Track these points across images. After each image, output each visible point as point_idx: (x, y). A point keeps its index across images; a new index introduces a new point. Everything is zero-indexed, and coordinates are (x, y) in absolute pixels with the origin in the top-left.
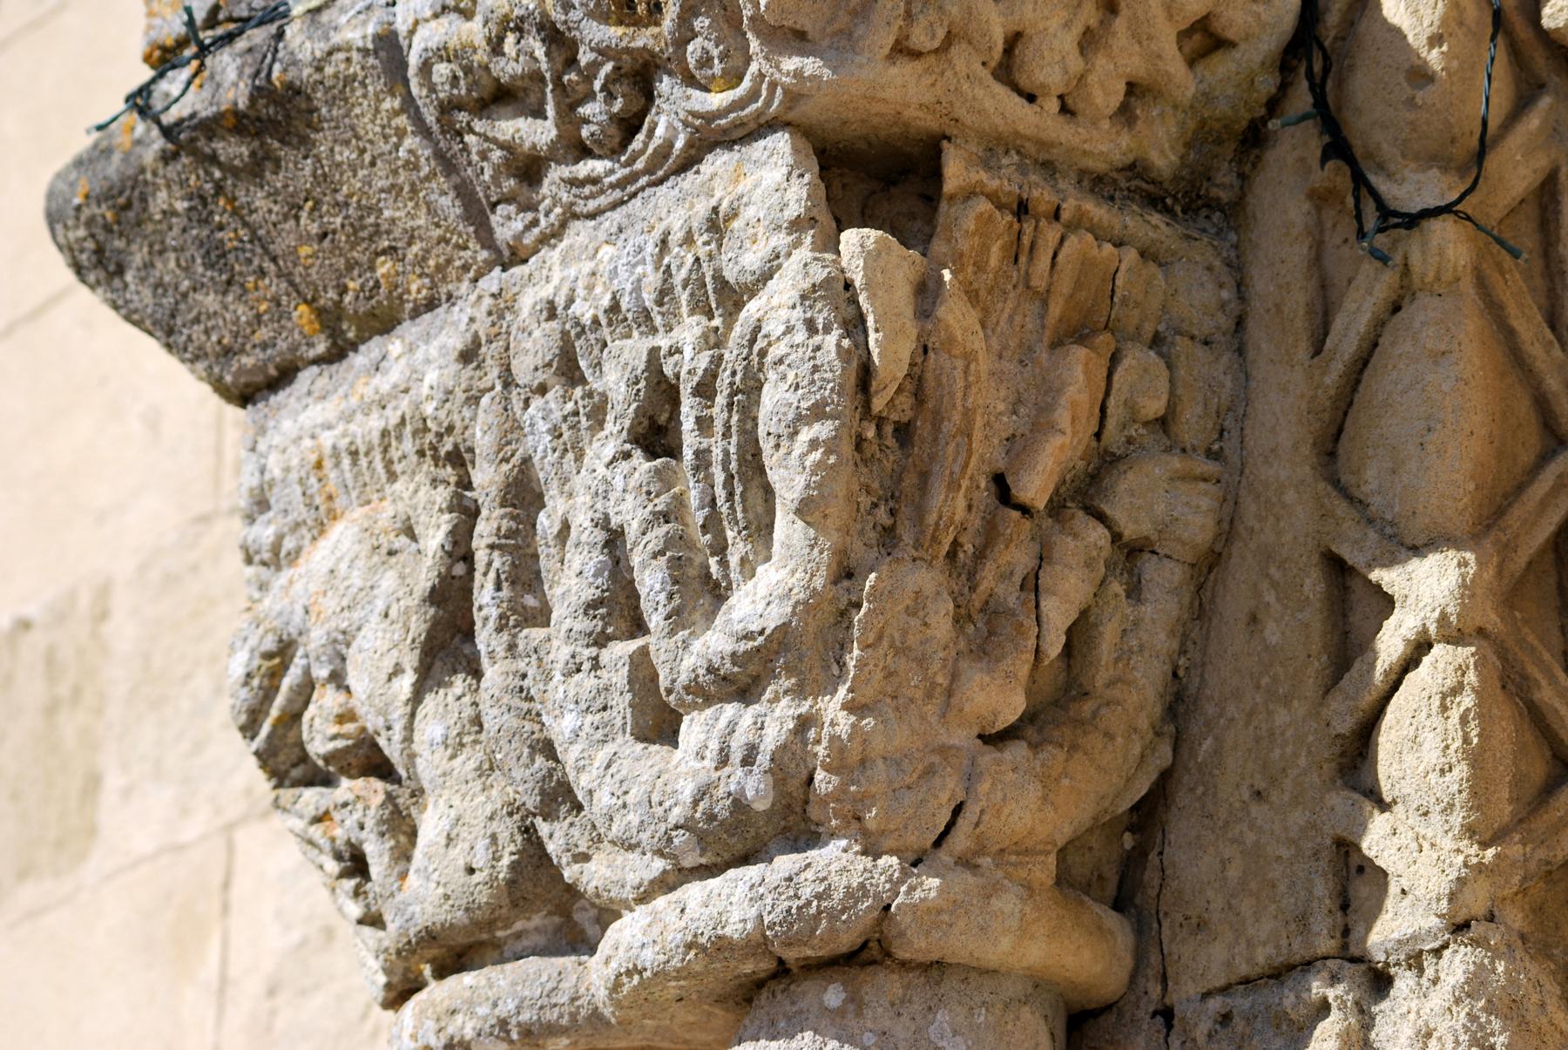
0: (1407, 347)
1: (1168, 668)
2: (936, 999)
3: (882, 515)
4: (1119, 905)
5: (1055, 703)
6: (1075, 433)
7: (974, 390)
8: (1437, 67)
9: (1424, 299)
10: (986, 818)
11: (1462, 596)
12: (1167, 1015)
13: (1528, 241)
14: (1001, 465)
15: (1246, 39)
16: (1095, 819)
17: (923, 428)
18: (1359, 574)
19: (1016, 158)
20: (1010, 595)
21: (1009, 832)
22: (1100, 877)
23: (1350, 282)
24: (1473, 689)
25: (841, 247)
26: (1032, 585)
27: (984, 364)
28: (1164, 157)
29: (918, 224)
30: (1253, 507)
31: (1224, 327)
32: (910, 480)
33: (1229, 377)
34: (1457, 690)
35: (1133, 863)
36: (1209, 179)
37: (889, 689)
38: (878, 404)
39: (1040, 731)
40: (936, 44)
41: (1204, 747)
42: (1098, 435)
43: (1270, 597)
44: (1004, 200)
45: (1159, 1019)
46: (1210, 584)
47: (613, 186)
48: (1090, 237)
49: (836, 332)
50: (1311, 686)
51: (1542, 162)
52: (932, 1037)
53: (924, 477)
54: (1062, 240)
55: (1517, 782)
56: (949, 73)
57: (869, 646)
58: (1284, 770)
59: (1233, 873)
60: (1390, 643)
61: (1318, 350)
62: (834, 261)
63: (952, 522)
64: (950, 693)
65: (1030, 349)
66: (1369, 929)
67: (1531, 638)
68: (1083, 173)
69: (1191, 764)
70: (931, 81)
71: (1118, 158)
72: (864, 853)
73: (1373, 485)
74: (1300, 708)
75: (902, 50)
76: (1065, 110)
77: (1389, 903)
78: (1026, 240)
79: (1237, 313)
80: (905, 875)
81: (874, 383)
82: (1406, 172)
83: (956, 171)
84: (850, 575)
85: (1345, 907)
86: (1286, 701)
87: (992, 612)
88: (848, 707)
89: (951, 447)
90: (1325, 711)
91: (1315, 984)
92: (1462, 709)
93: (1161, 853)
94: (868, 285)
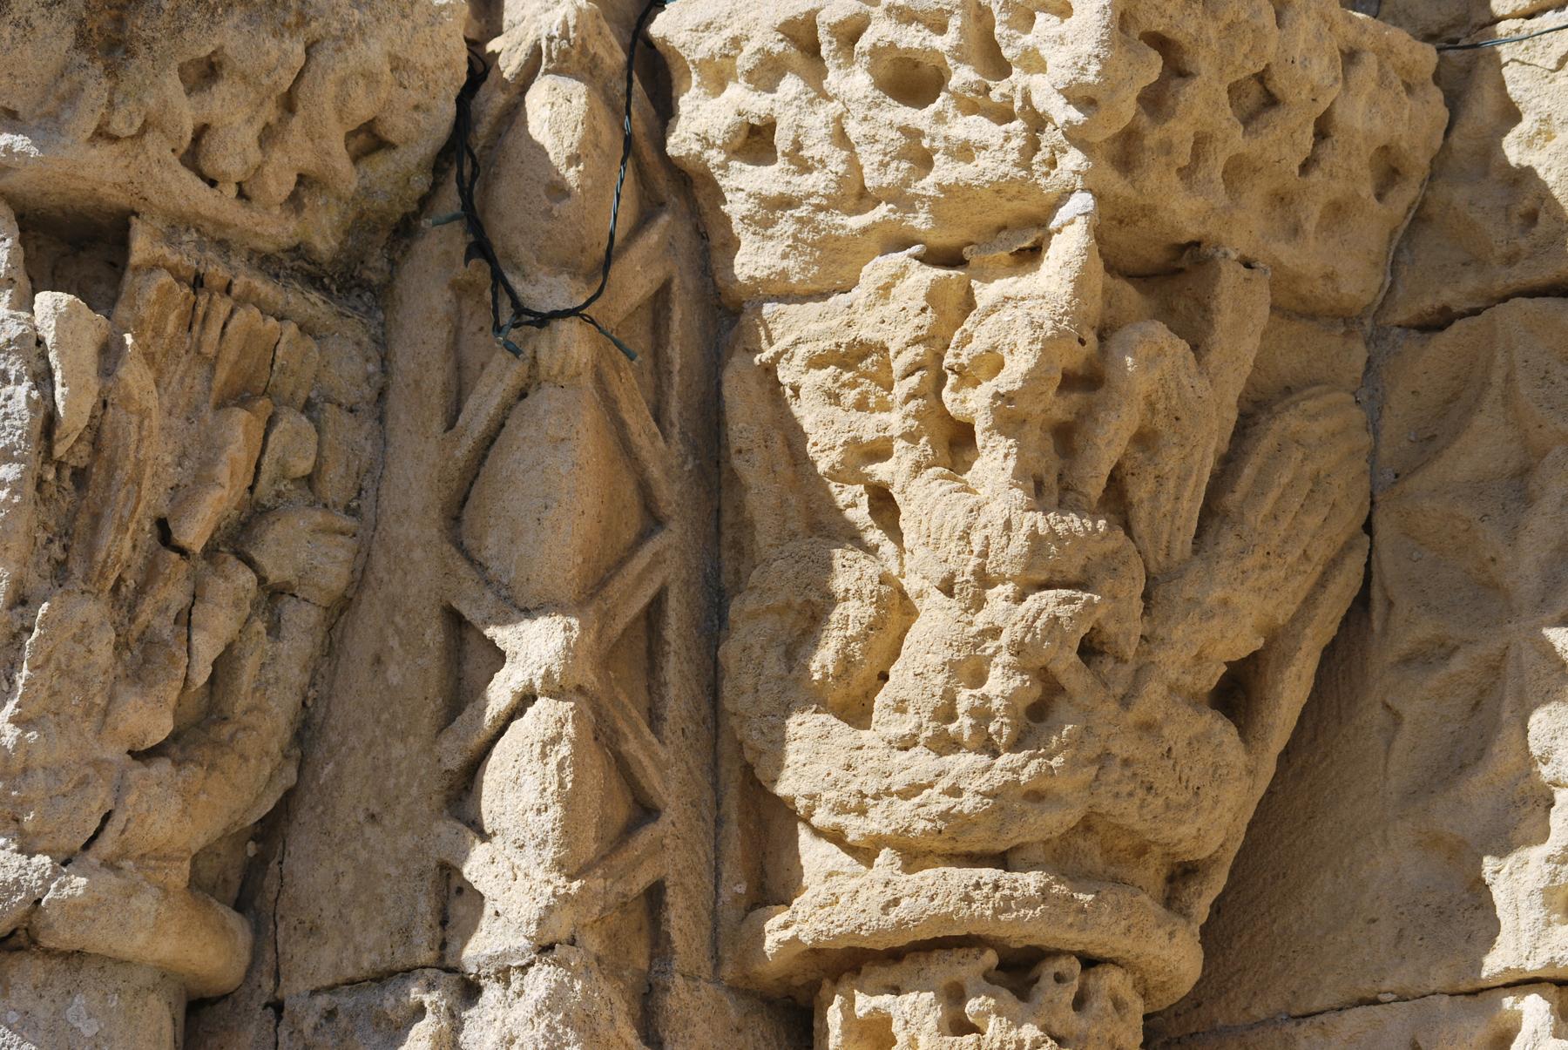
0: (532, 431)
1: (299, 699)
2: (75, 984)
3: (56, 549)
4: (240, 906)
5: (197, 725)
6: (232, 487)
7: (146, 443)
8: (574, 185)
9: (548, 389)
10: (131, 826)
11: (566, 657)
12: (278, 1007)
13: (641, 341)
14: (165, 511)
15: (406, 143)
16: (225, 830)
17: (98, 474)
18: (474, 627)
19: (195, 235)
20: (165, 628)
21: (150, 839)
22: (225, 881)
23: (483, 367)
24: (570, 740)
25: (35, 307)
26: (185, 620)
27: (156, 420)
28: (325, 243)
29: (102, 288)
30: (383, 561)
31: (368, 397)
32: (83, 520)
33: (370, 442)
34: (556, 740)
35: (254, 870)
36: (362, 262)
37: (53, 707)
38: (60, 450)
39: (183, 749)
40: (133, 131)
41: (326, 771)
42: (251, 489)
43: (394, 642)
44: (183, 273)
45: (270, 1010)
46: (340, 625)
48: (256, 311)
49: (27, 384)
50: (426, 723)
51: (658, 274)
52: (69, 1019)
53: (96, 518)
54: (232, 312)
55: (603, 823)
56: (142, 157)
57: (37, 667)
58: (397, 797)
59: (346, 885)
60: (500, 693)
61: (451, 425)
62: (28, 319)
63: (118, 557)
64: (106, 713)
65: (197, 408)
66: (464, 944)
67: (623, 697)
68: (253, 252)
69: (313, 785)
70: (126, 163)
71: (285, 241)
72: (20, 851)
73: (493, 552)
74: (415, 744)
75: (102, 134)
76: (242, 195)
77: (484, 923)
78: (200, 311)
79: (380, 385)
80: (56, 873)
81: (57, 432)
82: (540, 274)
83: (142, 246)
84: (24, 602)
85: (444, 923)
86: (403, 736)
87: (148, 642)
88: (15, 721)
89: (122, 494)
90: (437, 748)
91: (414, 990)
92: (559, 757)
93: (281, 863)
94: (58, 344)
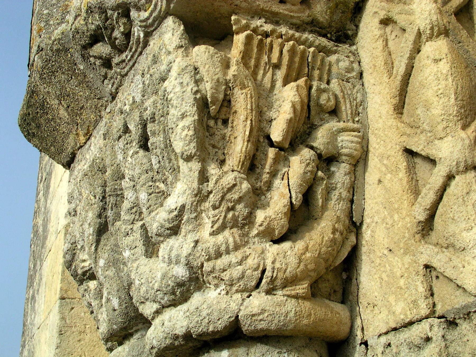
47: (130, 60)
93: (356, 279)
